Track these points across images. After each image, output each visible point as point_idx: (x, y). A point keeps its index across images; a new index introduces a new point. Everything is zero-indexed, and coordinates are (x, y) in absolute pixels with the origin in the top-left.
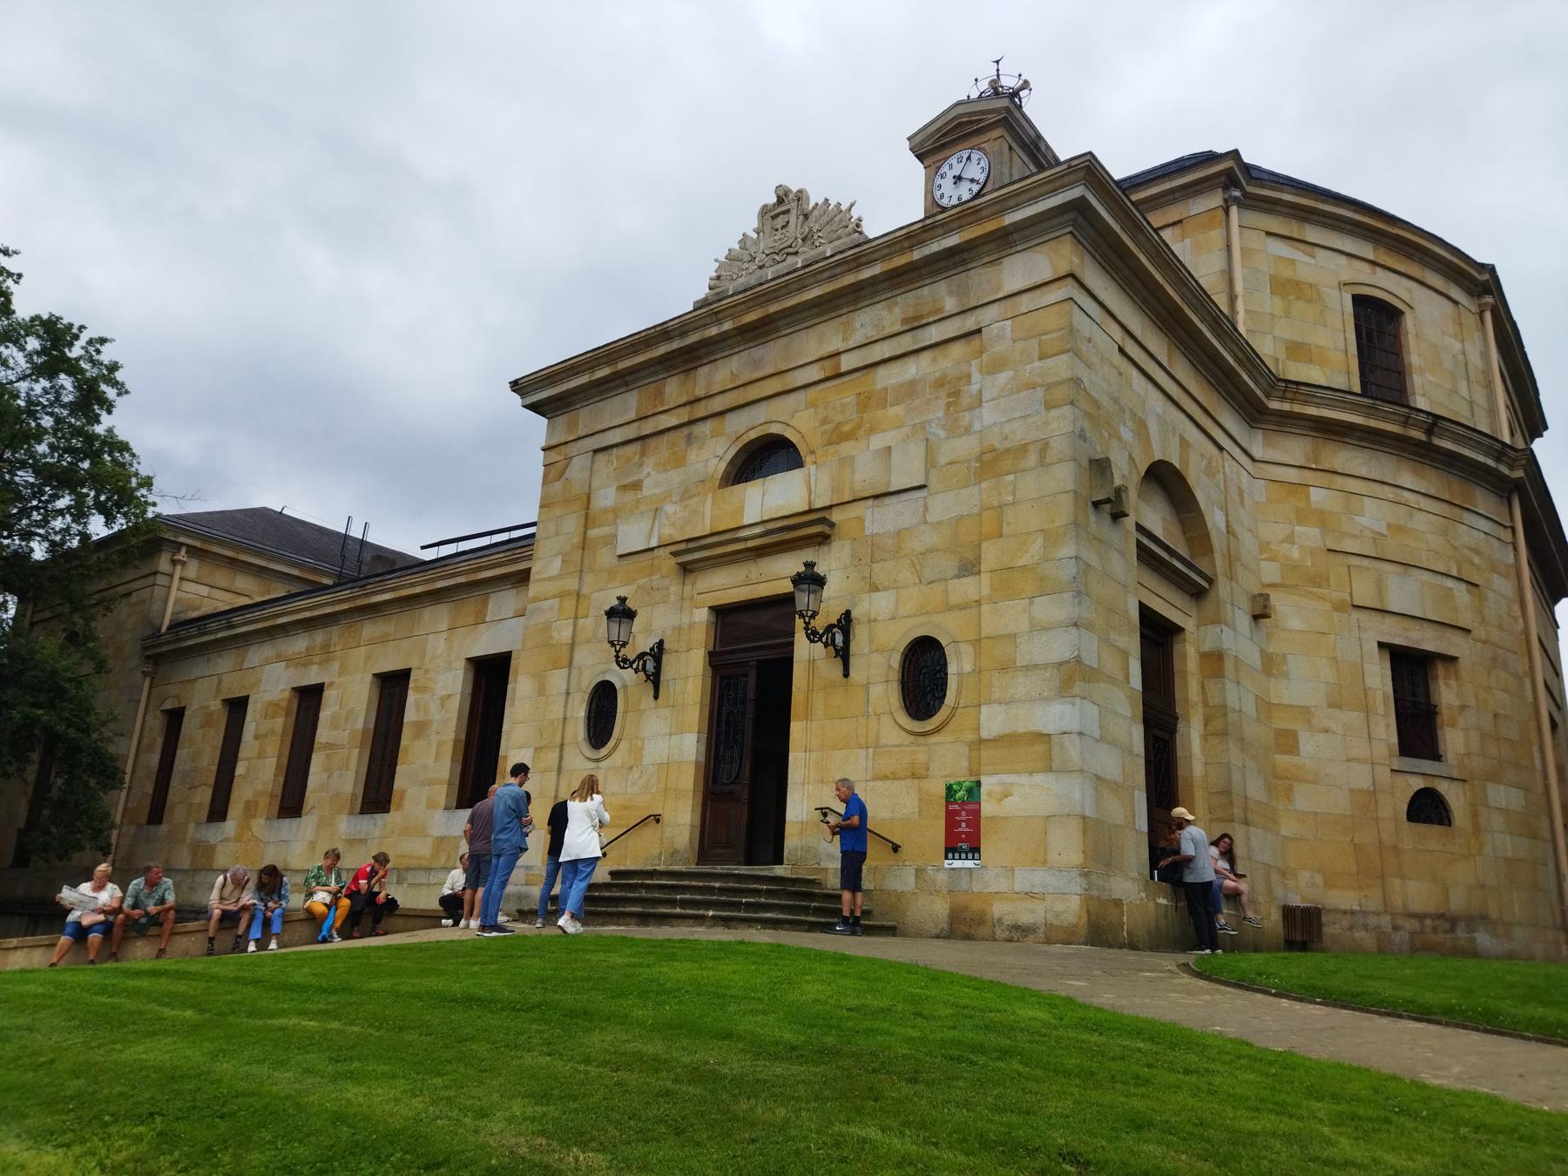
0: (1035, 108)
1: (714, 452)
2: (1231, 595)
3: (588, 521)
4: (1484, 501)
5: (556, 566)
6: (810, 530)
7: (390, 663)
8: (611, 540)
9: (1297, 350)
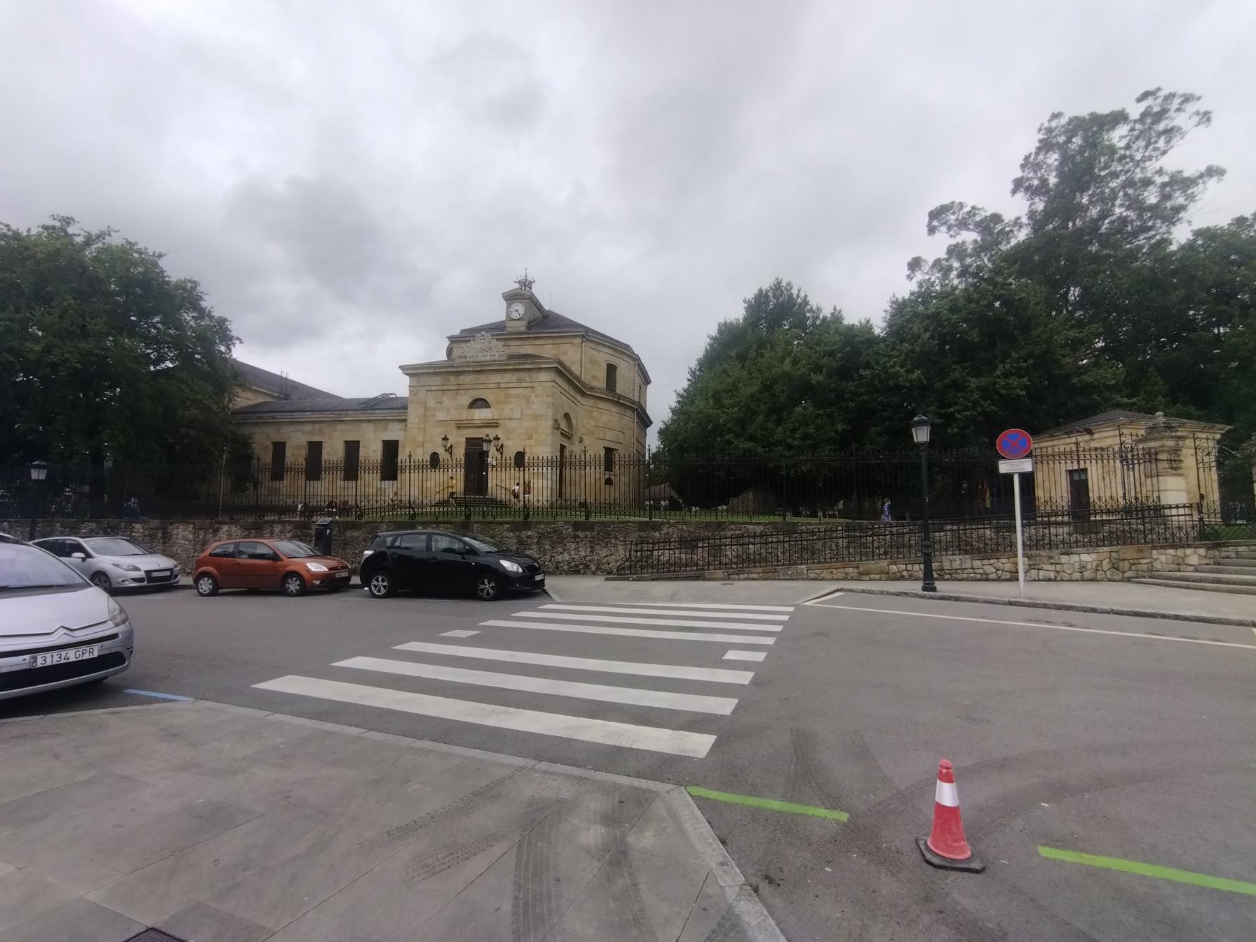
0: (536, 291)
1: (466, 399)
2: (576, 439)
3: (426, 409)
4: (629, 413)
5: (416, 420)
6: (494, 424)
7: (351, 437)
8: (434, 416)
9: (594, 378)
